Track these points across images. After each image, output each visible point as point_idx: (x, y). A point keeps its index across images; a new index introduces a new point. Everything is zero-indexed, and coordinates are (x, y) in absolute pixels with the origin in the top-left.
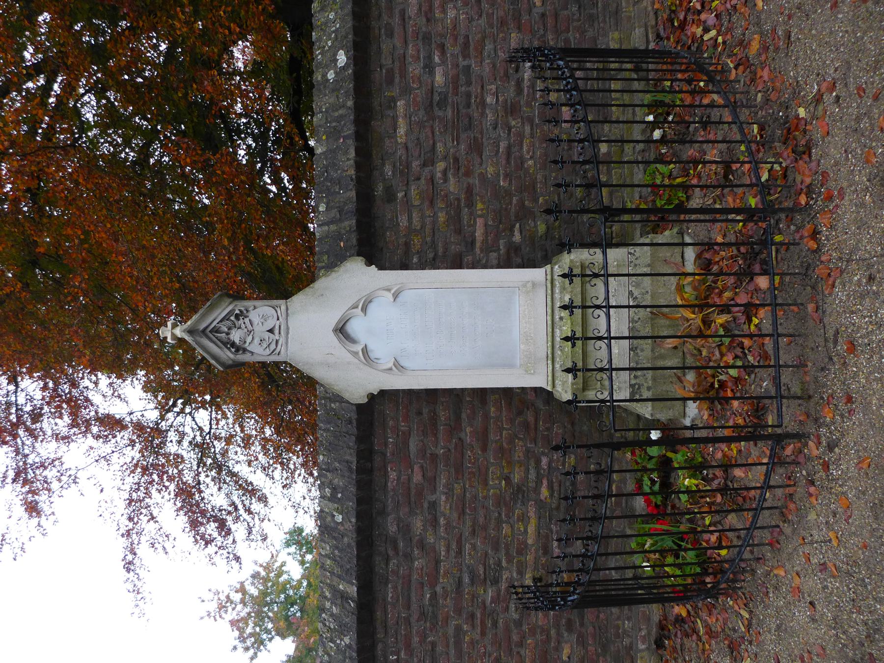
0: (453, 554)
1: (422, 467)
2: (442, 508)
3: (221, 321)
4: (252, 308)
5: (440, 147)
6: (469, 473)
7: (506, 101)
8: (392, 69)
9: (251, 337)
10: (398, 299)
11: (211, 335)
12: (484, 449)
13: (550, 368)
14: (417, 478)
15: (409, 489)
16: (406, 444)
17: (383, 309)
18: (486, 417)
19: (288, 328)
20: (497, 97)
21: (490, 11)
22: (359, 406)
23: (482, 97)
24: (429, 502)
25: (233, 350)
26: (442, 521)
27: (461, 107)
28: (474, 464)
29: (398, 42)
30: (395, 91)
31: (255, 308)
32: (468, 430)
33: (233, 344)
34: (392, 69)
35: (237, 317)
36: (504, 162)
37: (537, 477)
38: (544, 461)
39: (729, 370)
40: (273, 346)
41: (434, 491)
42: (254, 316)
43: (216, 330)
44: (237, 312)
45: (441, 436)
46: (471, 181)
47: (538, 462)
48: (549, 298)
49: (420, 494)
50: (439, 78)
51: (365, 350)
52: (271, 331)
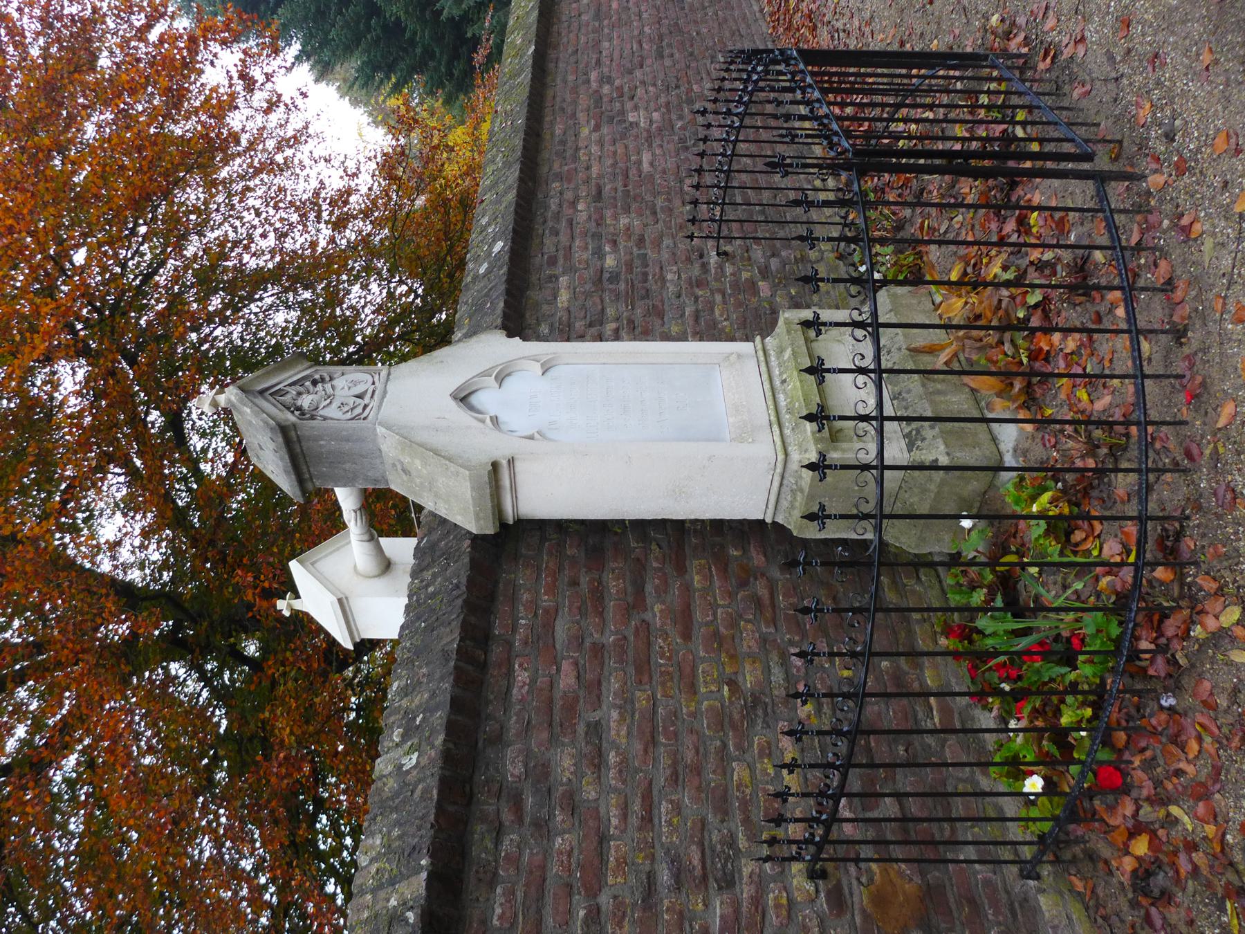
0: (634, 821)
3: (290, 385)
5: (610, 311)
24: (588, 725)
25: (297, 413)
33: (299, 409)
35: (315, 383)
50: (610, 261)
51: (495, 420)
52: (360, 396)
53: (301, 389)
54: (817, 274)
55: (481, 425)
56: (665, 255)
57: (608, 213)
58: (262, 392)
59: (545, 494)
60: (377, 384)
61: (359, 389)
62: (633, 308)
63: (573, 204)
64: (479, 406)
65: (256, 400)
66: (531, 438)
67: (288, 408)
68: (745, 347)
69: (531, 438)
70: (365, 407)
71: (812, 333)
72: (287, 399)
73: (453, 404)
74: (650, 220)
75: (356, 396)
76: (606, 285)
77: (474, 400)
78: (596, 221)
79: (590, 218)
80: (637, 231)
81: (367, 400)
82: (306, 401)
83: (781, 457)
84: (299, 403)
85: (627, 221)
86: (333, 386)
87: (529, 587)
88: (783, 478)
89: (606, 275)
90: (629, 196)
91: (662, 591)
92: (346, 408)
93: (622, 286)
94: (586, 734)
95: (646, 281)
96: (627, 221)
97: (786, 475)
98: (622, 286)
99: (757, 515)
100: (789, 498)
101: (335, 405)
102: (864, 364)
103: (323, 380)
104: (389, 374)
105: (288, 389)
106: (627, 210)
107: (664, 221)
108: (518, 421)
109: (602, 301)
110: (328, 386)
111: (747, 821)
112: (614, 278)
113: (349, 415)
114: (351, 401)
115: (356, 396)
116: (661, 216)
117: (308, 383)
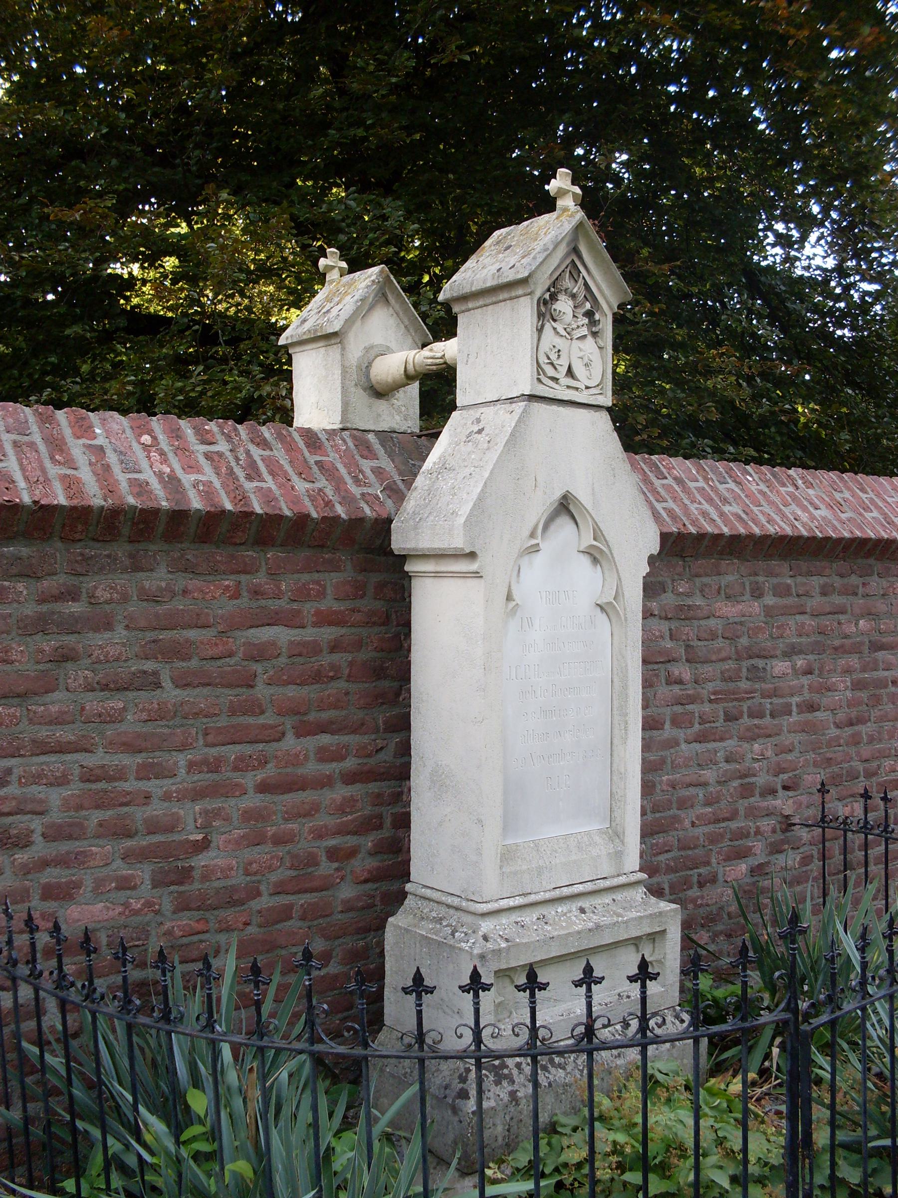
0: (43, 733)
3: (586, 284)
5: (707, 670)
7: (755, 775)
10: (599, 609)
11: (568, 261)
12: (264, 788)
13: (504, 904)
17: (587, 582)
18: (325, 782)
21: (842, 741)
22: (384, 526)
24: (155, 673)
25: (547, 296)
26: (116, 703)
27: (749, 702)
29: (816, 602)
30: (770, 600)
33: (554, 297)
34: (790, 595)
35: (589, 314)
36: (688, 780)
40: (550, 371)
41: (181, 682)
43: (574, 273)
44: (597, 317)
45: (292, 691)
46: (667, 726)
48: (589, 887)
49: (178, 652)
50: (780, 666)
51: (535, 549)
52: (570, 373)
53: (581, 297)
54: (596, 983)
55: (527, 533)
56: (787, 739)
57: (854, 661)
58: (576, 251)
59: (442, 613)
60: (586, 392)
61: (578, 370)
62: (710, 701)
63: (869, 614)
64: (553, 527)
65: (564, 245)
66: (509, 598)
67: (554, 284)
68: (632, 860)
69: (509, 598)
70: (555, 380)
71: (522, 980)
72: (567, 283)
73: (558, 494)
74: (841, 716)
75: (570, 367)
76: (745, 664)
77: (564, 521)
78: (842, 646)
79: (846, 637)
80: (825, 701)
81: (565, 381)
82: (564, 305)
83: (484, 908)
84: (562, 297)
85: (842, 686)
86: (584, 337)
87: (332, 584)
88: (457, 909)
89: (760, 663)
90: (877, 687)
91: (324, 755)
92: (553, 357)
93: (744, 685)
94: (145, 672)
95: (751, 715)
96: (842, 686)
97: (459, 914)
98: (744, 685)
99: (434, 857)
100: (434, 914)
101: (558, 341)
102: (486, 1034)
103: (593, 323)
104: (598, 407)
105: (581, 281)
106: (858, 686)
107: (838, 737)
108: (535, 576)
109: (723, 660)
110: (584, 331)
111: (44, 864)
112: (756, 674)
113: (543, 360)
114: (563, 363)
115: (570, 367)
116: (849, 731)
117: (588, 306)
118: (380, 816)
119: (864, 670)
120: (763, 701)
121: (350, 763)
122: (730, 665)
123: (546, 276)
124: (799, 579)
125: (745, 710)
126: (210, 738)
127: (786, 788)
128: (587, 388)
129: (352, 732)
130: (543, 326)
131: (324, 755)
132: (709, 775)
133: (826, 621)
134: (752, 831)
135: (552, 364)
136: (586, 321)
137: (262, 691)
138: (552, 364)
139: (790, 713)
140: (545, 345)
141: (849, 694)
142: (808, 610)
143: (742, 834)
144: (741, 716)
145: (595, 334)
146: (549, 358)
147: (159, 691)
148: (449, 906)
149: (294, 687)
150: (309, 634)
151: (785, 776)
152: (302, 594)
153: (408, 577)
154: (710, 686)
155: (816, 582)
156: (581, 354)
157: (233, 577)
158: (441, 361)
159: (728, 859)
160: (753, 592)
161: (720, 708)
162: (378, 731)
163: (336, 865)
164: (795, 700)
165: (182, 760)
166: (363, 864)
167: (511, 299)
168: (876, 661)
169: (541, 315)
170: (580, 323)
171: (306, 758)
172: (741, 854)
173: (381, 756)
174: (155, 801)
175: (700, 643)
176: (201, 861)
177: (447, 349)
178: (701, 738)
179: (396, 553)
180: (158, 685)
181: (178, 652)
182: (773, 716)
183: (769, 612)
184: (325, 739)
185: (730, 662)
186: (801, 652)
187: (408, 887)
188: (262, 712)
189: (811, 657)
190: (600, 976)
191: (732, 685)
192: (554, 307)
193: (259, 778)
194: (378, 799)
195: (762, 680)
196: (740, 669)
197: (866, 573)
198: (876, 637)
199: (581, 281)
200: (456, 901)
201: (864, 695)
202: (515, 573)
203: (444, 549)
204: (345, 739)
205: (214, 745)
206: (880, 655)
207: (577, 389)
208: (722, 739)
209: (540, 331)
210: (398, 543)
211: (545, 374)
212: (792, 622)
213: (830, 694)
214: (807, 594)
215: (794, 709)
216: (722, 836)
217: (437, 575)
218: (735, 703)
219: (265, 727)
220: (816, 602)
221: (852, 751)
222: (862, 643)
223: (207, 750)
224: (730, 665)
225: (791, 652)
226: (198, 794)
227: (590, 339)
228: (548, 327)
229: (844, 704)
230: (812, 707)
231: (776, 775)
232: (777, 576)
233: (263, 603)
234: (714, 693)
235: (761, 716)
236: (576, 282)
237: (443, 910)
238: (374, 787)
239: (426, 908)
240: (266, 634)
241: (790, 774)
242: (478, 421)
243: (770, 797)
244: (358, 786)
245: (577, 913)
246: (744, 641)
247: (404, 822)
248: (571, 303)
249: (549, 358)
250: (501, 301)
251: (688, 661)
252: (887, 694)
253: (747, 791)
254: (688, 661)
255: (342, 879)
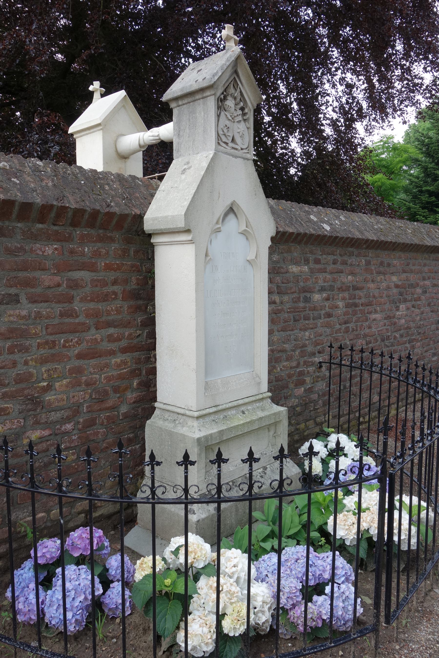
1: (59, 285)
2: (12, 312)
3: (241, 92)
4: (248, 126)
5: (286, 298)
6: (54, 342)
7: (306, 347)
8: (320, 263)
9: (230, 118)
11: (232, 78)
12: (80, 356)
14: (47, 279)
15: (35, 269)
16: (83, 267)
18: (112, 353)
19: (236, 157)
20: (308, 340)
23: (308, 329)
24: (17, 295)
25: (222, 97)
27: (304, 313)
28: (64, 346)
29: (330, 267)
30: (312, 265)
31: (248, 128)
32: (98, 337)
33: (225, 98)
34: (320, 263)
35: (242, 109)
36: (279, 349)
37: (53, 423)
38: (69, 427)
39: (16, 595)
40: (224, 139)
41: (33, 300)
42: (242, 126)
45: (92, 305)
47: (68, 420)
49: (28, 283)
50: (317, 297)
51: (218, 231)
52: (233, 140)
53: (238, 100)
55: (215, 221)
56: (320, 330)
57: (346, 295)
60: (241, 151)
61: (238, 139)
62: (288, 312)
63: (352, 273)
66: (207, 255)
67: (225, 90)
68: (265, 386)
70: (226, 144)
72: (231, 90)
76: (302, 295)
82: (230, 103)
84: (229, 98)
88: (183, 415)
89: (308, 295)
91: (111, 339)
92: (225, 131)
93: (301, 305)
94: (10, 294)
98: (301, 305)
101: (228, 123)
103: (244, 114)
105: (238, 90)
110: (240, 118)
112: (307, 300)
113: (221, 132)
117: (242, 104)
118: (140, 370)
119: (350, 299)
120: (309, 312)
121: (124, 343)
122: (295, 295)
123: (222, 85)
124: (324, 256)
125: (302, 316)
126: (49, 330)
127: (319, 352)
128: (242, 149)
129: (125, 327)
130: (220, 113)
131: (111, 339)
132: (287, 346)
133: (335, 276)
134: (306, 372)
135: (225, 135)
136: (240, 112)
137: (77, 306)
138: (225, 135)
139: (320, 318)
140: (221, 125)
141: (344, 310)
142: (328, 271)
143: (301, 373)
144: (301, 319)
145: (245, 120)
146: (223, 132)
147: (19, 304)
148: (178, 414)
149: (94, 303)
150: (101, 275)
151: (319, 347)
152: (97, 254)
153: (152, 246)
154: (288, 305)
155: (331, 258)
156: (239, 131)
157: (59, 243)
158: (157, 138)
159: (296, 385)
160: (305, 261)
161: (291, 315)
162: (138, 326)
163: (118, 395)
164: (323, 312)
165: (34, 343)
166: (131, 396)
167: (203, 98)
168: (355, 295)
169: (219, 108)
170: (239, 113)
171: (102, 340)
172: (303, 383)
173: (139, 339)
174: (19, 366)
175: (283, 285)
176: (49, 397)
177: (165, 131)
178: (284, 330)
179: (147, 233)
180: (18, 302)
181: (28, 283)
182: (314, 319)
183: (312, 271)
184: (111, 331)
185: (296, 294)
186: (325, 290)
187: (156, 405)
188: (77, 316)
189: (329, 293)
190: (317, 451)
191: (296, 305)
192: (225, 103)
193: (76, 352)
194: (138, 361)
195: (309, 302)
196: (300, 297)
197: (351, 254)
198: (355, 283)
199: (238, 90)
200: (182, 411)
201: (350, 310)
202: (209, 243)
203: (174, 228)
204: (121, 330)
205: (51, 334)
206: (357, 292)
207: (237, 149)
208: (292, 330)
209: (219, 116)
210: (149, 224)
211: (222, 141)
212: (321, 276)
213: (337, 309)
214: (327, 263)
215: (322, 316)
216: (293, 375)
217: (171, 243)
218: (298, 313)
219: (79, 324)
220: (330, 267)
221: (346, 335)
222: (350, 287)
223: (47, 337)
224: (295, 295)
225: (322, 289)
226: (44, 361)
227: (242, 122)
228: (222, 113)
229: (342, 314)
230: (329, 315)
231: (315, 346)
232: (315, 254)
233: (75, 258)
234: (289, 309)
235: (308, 319)
236: (236, 90)
237: (176, 416)
238: (136, 354)
239: (167, 415)
240: (78, 275)
241: (321, 346)
242: (188, 163)
243: (313, 357)
244: (128, 354)
245: (241, 414)
246: (302, 284)
247: (153, 372)
248: (233, 102)
249: (223, 132)
250: (197, 100)
251: (278, 293)
252: (359, 310)
253: (303, 354)
254: (278, 293)
255: (122, 402)
